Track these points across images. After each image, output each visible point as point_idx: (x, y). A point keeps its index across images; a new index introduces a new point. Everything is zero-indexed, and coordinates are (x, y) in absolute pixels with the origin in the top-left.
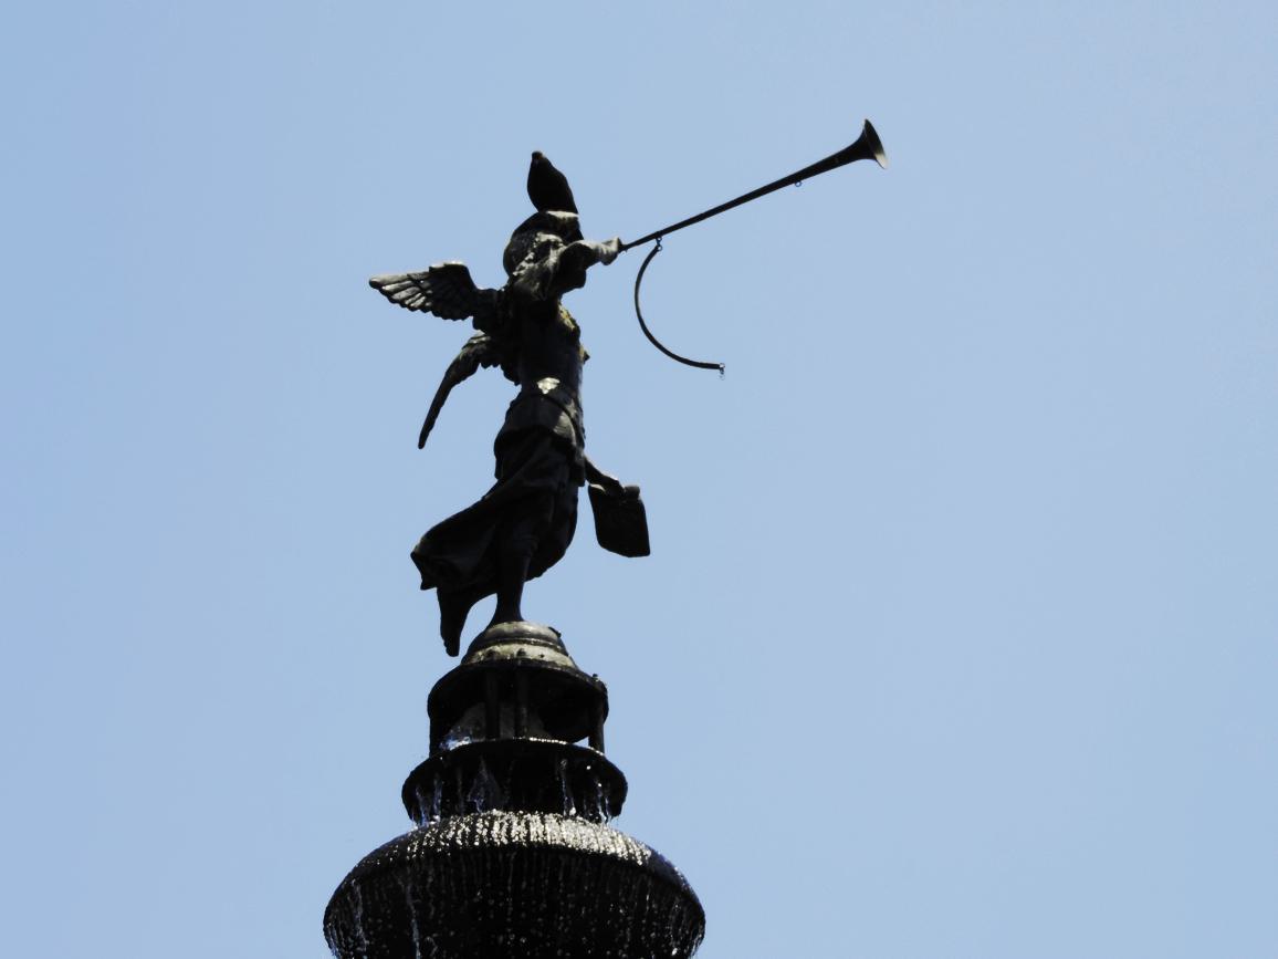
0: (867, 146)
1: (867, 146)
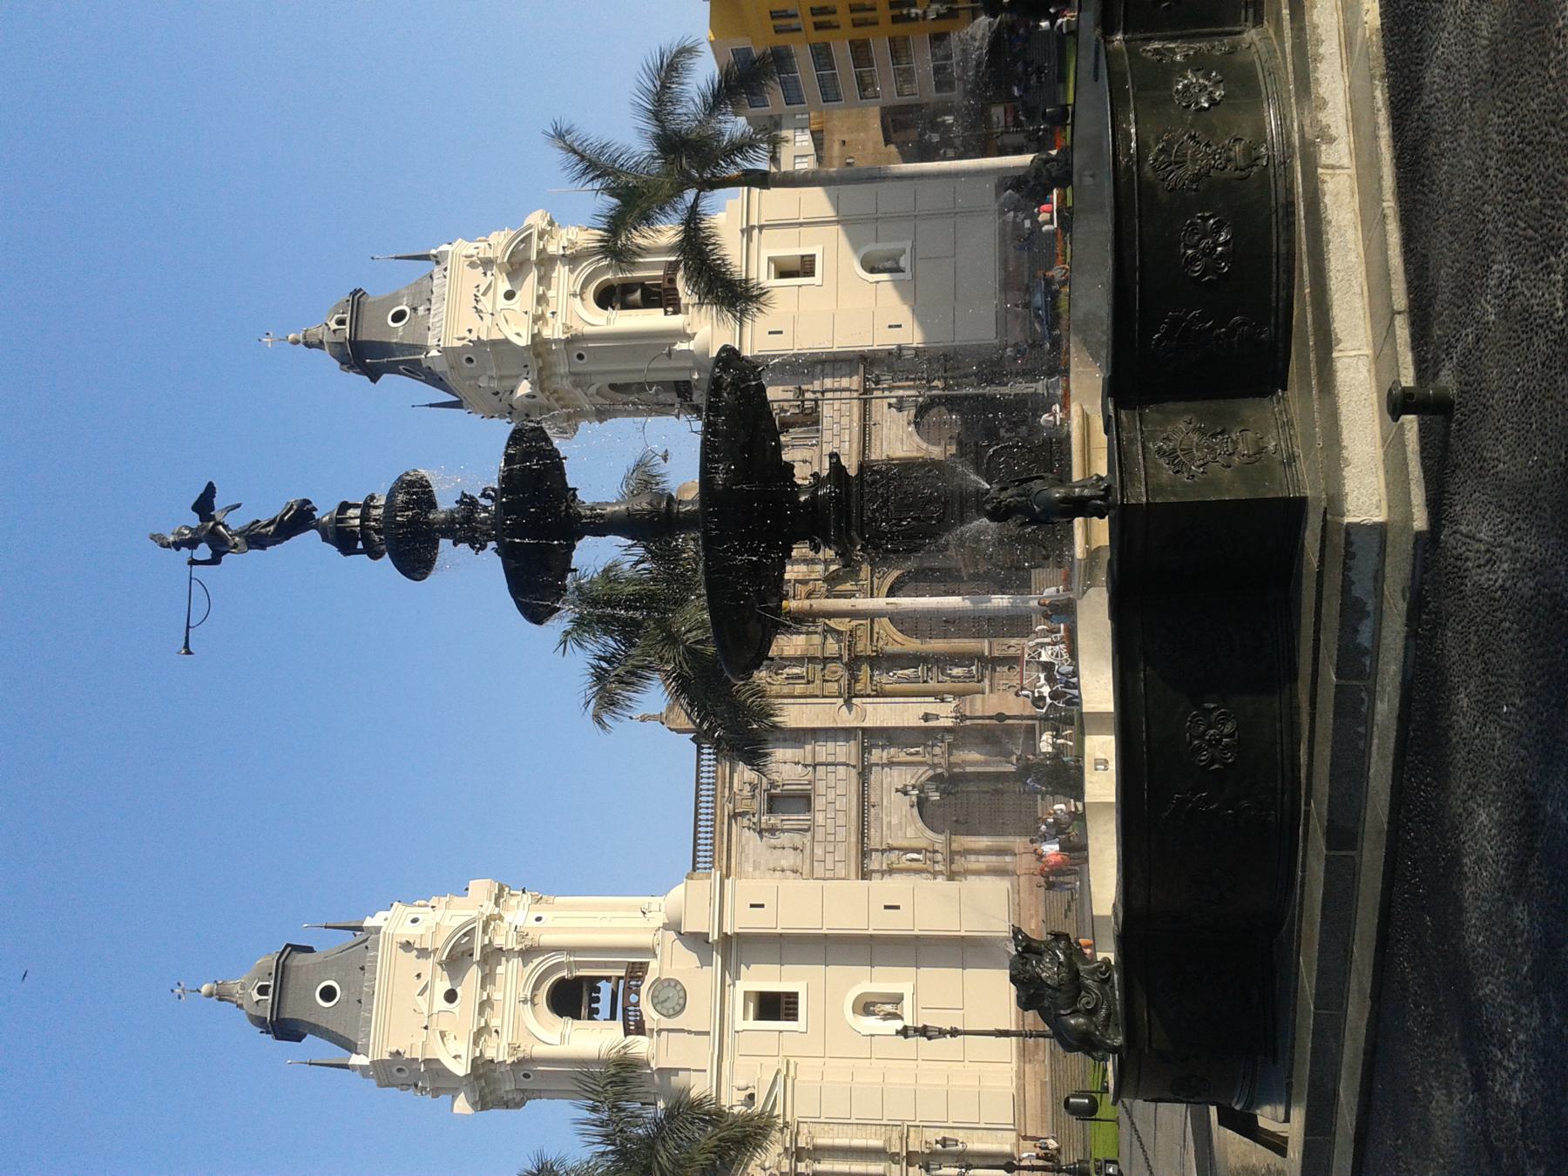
0: (189, 653)
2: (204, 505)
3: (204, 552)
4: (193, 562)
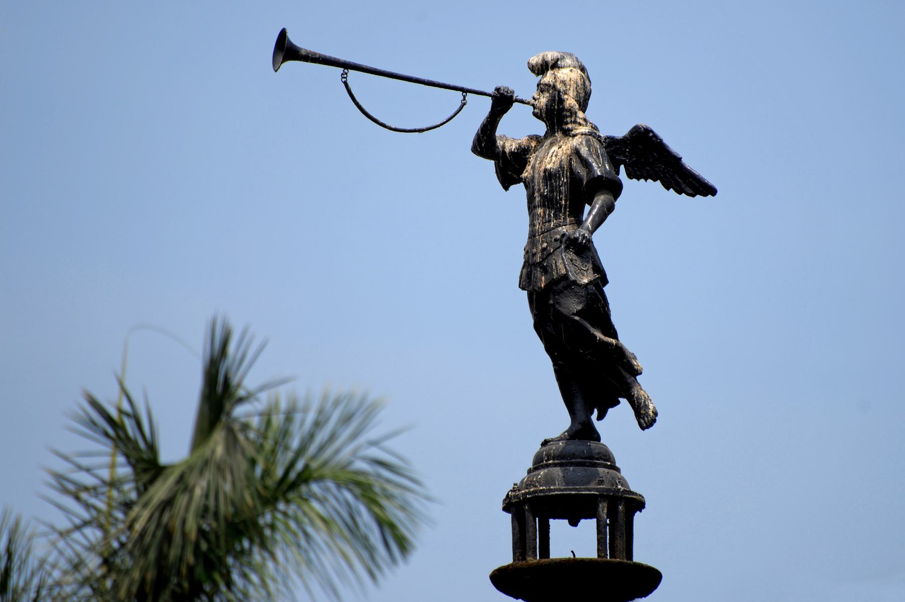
0: (286, 50)
1: (286, 50)
2: (645, 155)
3: (518, 127)
4: (502, 102)
